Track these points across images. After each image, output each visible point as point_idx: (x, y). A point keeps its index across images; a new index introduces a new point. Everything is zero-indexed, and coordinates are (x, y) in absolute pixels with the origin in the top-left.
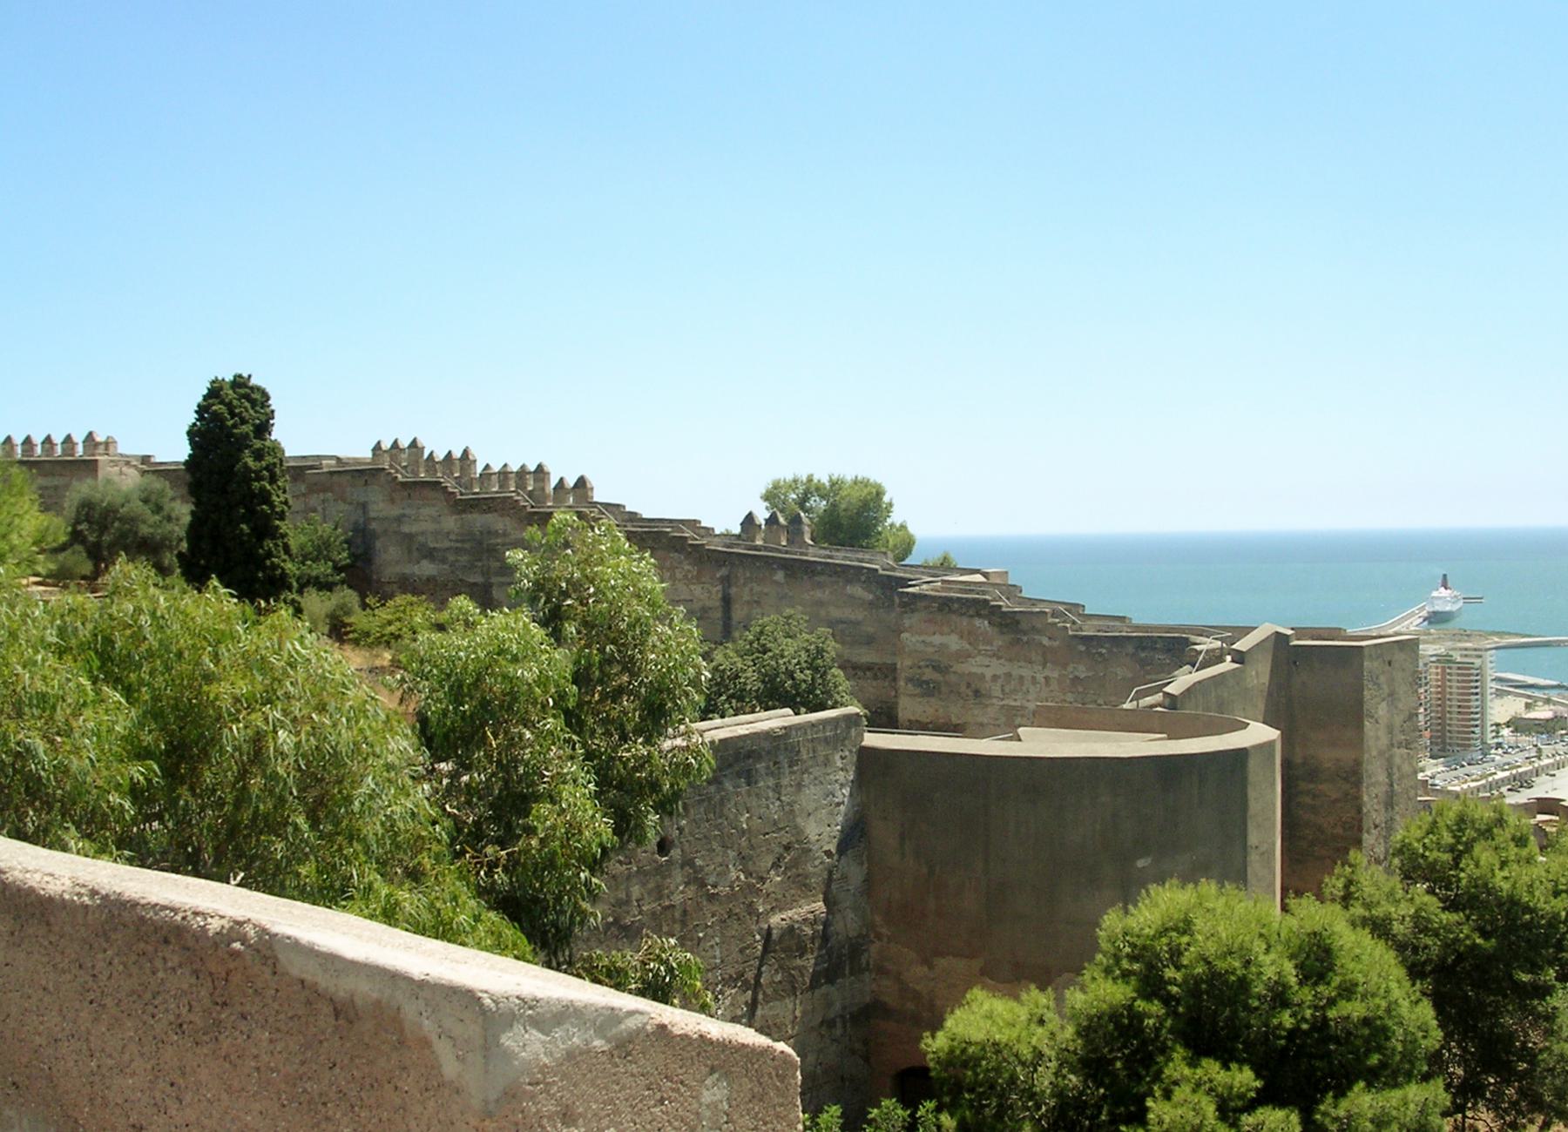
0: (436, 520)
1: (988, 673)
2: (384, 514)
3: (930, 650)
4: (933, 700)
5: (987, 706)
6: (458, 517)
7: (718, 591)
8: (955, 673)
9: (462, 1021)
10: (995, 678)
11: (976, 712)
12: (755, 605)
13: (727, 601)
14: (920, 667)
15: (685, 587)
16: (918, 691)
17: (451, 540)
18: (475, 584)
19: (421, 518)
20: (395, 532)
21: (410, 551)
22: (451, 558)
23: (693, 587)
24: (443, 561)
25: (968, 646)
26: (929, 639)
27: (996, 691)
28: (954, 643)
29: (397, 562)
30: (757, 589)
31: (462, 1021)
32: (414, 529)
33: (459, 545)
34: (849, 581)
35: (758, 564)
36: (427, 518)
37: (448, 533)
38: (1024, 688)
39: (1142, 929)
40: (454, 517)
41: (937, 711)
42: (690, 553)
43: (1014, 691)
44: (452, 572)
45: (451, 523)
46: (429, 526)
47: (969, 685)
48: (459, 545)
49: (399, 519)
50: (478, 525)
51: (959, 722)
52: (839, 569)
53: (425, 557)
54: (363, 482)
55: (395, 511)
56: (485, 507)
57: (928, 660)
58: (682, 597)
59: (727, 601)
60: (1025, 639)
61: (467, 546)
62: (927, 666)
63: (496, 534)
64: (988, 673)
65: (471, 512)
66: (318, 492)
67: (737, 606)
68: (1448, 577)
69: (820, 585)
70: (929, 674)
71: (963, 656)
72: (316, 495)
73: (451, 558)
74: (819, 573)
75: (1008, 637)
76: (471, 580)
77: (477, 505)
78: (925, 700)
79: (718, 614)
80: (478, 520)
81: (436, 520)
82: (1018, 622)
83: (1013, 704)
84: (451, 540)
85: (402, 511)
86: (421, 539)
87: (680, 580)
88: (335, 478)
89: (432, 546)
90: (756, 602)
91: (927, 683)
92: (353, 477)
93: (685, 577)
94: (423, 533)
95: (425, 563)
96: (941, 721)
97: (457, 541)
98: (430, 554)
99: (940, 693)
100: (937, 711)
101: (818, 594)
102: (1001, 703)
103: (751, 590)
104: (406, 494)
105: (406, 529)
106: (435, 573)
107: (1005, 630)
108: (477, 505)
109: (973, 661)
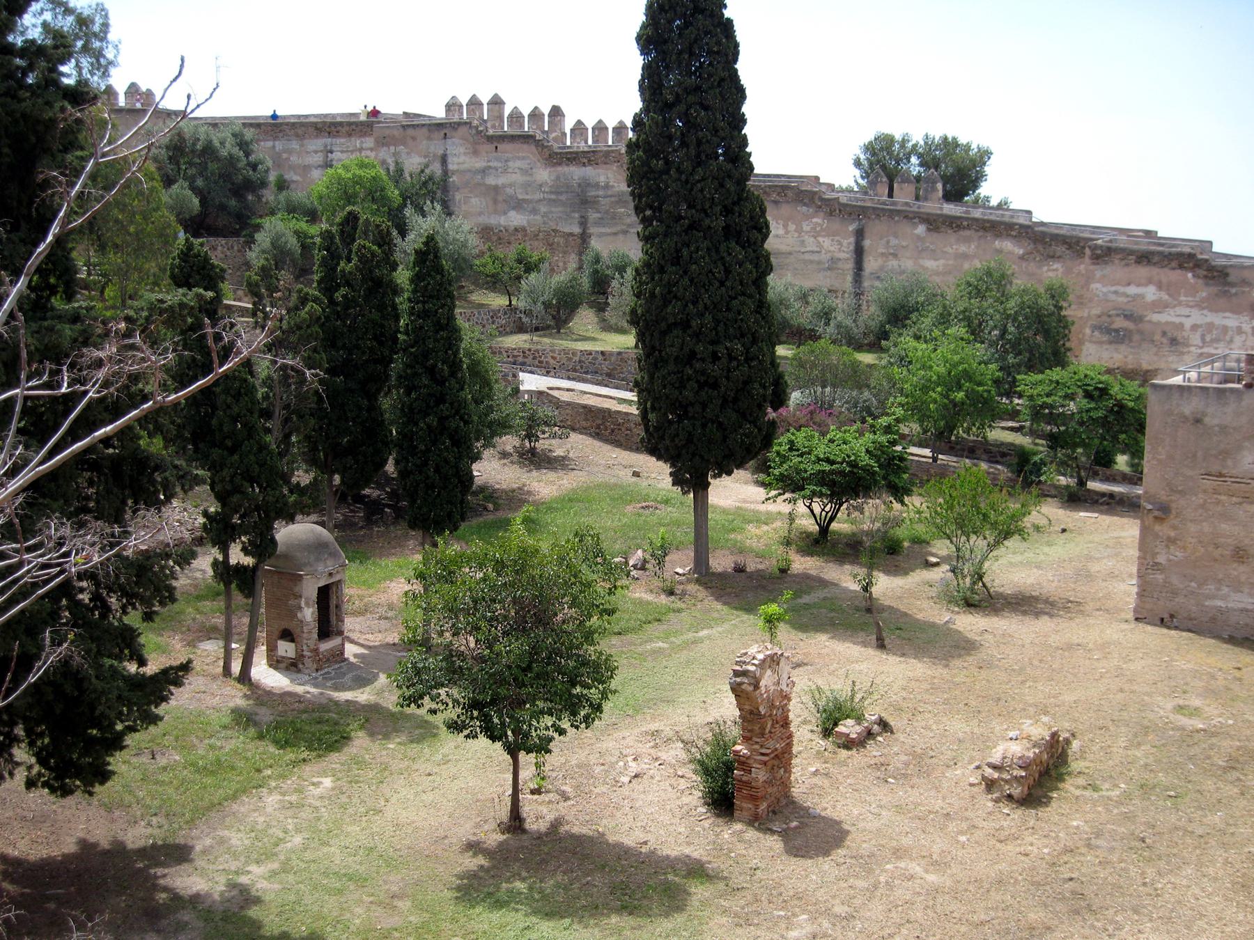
0: (525, 172)
1: (1188, 323)
2: (466, 166)
3: (1121, 299)
4: (1122, 348)
5: (1183, 353)
6: (552, 169)
7: (849, 244)
8: (1150, 322)
9: (1064, 531)
10: (1195, 327)
11: (1170, 359)
12: (891, 257)
13: (859, 252)
14: (1109, 316)
15: (812, 239)
16: (1105, 338)
17: (544, 192)
18: (571, 234)
19: (510, 170)
20: (479, 184)
21: (495, 202)
22: (543, 209)
23: (821, 239)
24: (534, 211)
25: (1166, 297)
26: (1121, 289)
27: (1196, 339)
28: (1151, 293)
29: (480, 214)
30: (894, 242)
31: (1064, 531)
32: (500, 181)
33: (553, 197)
34: (999, 235)
35: (896, 218)
36: (516, 170)
37: (541, 186)
38: (1228, 338)
39: (269, 826)
40: (548, 170)
41: (1126, 357)
42: (820, 207)
43: (1217, 340)
44: (544, 223)
45: (544, 175)
46: (518, 178)
47: (1164, 334)
48: (553, 197)
49: (484, 171)
50: (576, 178)
51: (1150, 368)
52: (988, 225)
53: (514, 208)
54: (442, 135)
55: (479, 164)
56: (586, 161)
57: (1120, 309)
58: (808, 249)
59: (859, 252)
60: (1233, 291)
61: (563, 197)
62: (1118, 315)
63: (597, 186)
64: (1188, 323)
65: (568, 165)
66: (388, 145)
67: (871, 258)
68: (186, 59)
69: (967, 240)
70: (1120, 323)
71: (1159, 306)
72: (385, 148)
73: (543, 209)
74: (964, 228)
75: (1214, 290)
76: (567, 230)
77: (574, 159)
78: (1113, 347)
79: (850, 265)
80: (576, 173)
81: (525, 172)
82: (1227, 275)
83: (1213, 351)
84: (544, 192)
85: (485, 164)
86: (509, 191)
87: (807, 232)
88: (410, 132)
89: (520, 197)
90: (891, 254)
91: (1117, 331)
92: (429, 130)
93: (814, 229)
94: (511, 185)
95: (512, 214)
96: (1130, 367)
97: (551, 192)
98: (518, 205)
99: (1131, 341)
100: (1126, 357)
101: (963, 248)
102: (1200, 351)
103: (888, 242)
104: (494, 146)
105: (491, 181)
106: (525, 223)
107: (1211, 282)
108: (574, 159)
109: (1172, 312)
